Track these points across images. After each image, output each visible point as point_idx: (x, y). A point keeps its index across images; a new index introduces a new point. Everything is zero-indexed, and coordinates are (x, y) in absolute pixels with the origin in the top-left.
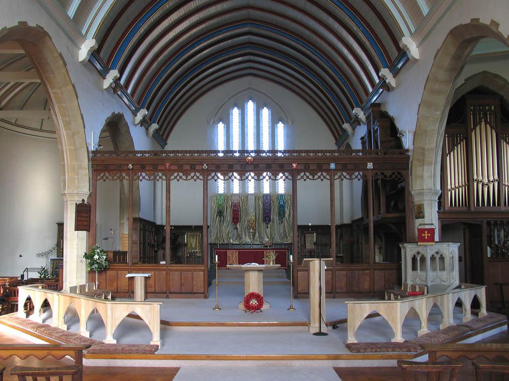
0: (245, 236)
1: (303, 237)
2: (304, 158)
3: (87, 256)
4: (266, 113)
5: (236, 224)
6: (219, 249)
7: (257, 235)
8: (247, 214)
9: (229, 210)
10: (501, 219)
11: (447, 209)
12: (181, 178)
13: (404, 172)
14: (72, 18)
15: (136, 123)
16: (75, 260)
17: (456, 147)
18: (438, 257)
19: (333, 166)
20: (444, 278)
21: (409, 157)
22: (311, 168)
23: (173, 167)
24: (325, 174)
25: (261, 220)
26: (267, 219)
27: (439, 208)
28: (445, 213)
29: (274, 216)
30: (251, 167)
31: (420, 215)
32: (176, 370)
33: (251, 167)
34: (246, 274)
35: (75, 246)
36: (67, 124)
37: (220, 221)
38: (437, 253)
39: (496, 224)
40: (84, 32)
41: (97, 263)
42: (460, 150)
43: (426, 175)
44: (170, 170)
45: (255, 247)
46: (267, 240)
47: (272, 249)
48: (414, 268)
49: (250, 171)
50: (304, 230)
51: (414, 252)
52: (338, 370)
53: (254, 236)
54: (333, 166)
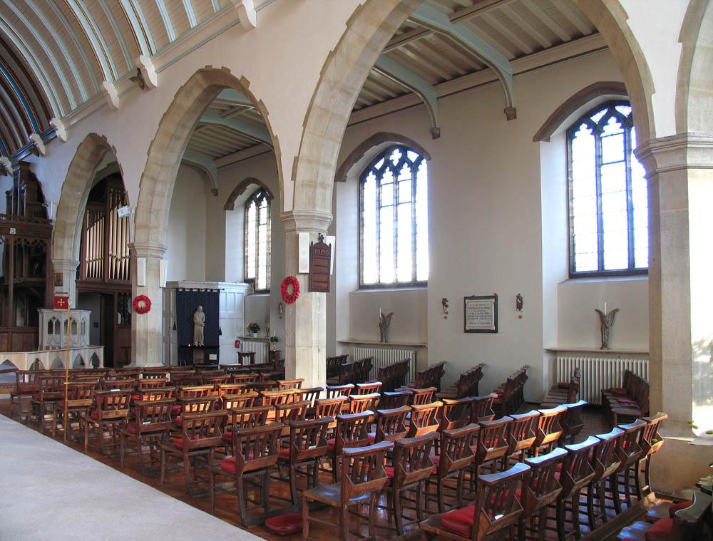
11: (84, 279)
27: (77, 278)
28: (82, 282)
31: (59, 282)
43: (66, 246)
48: (50, 332)
51: (50, 317)
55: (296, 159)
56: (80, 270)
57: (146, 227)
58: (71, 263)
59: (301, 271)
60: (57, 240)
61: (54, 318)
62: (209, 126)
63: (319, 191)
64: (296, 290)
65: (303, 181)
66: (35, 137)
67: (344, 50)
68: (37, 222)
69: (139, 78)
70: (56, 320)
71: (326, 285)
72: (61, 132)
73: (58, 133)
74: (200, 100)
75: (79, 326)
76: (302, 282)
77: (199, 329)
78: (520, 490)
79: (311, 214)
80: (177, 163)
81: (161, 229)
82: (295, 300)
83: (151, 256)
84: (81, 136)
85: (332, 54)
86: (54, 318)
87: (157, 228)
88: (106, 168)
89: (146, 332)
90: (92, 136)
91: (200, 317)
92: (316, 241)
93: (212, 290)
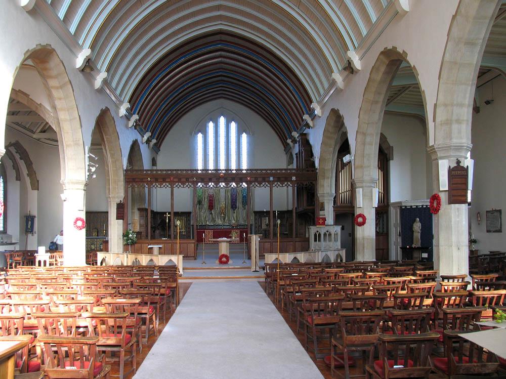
0: (218, 219)
1: (260, 219)
2: (255, 174)
3: (124, 236)
4: (233, 125)
5: (211, 210)
6: (199, 229)
7: (227, 218)
8: (219, 202)
9: (206, 200)
11: (338, 204)
12: (180, 186)
13: (314, 182)
14: (73, 34)
15: (144, 142)
16: (116, 237)
18: (328, 234)
19: (271, 179)
20: (331, 246)
21: (317, 173)
22: (259, 179)
23: (175, 180)
24: (267, 183)
25: (230, 207)
26: (234, 206)
29: (239, 204)
30: (223, 179)
31: (323, 209)
32: (191, 283)
33: (223, 180)
34: (220, 244)
35: (116, 229)
36: (112, 155)
37: (200, 208)
38: (327, 231)
40: (81, 42)
41: (131, 239)
43: (326, 185)
44: (173, 182)
45: (225, 227)
46: (234, 222)
47: (238, 229)
48: (315, 240)
49: (222, 182)
50: (260, 214)
51: (315, 231)
52: (259, 282)
53: (224, 219)
54: (271, 179)
55: (435, 105)
56: (336, 199)
57: (362, 167)
58: (329, 195)
59: (441, 189)
60: (320, 181)
61: (317, 232)
62: (414, 86)
63: (455, 127)
64: (439, 204)
65: (441, 121)
66: (306, 117)
67: (463, 11)
68: (308, 171)
69: (349, 68)
70: (328, 233)
71: (122, 212)
72: (318, 111)
73: (316, 112)
74: (386, 73)
75: (333, 236)
76: (444, 197)
77: (417, 235)
78: (483, 357)
79: (448, 145)
80: (379, 119)
81: (372, 167)
82: (438, 211)
83: (366, 186)
84: (327, 113)
85: (454, 17)
86: (317, 232)
89: (363, 238)
90: (333, 110)
91: (417, 226)
92: (454, 165)
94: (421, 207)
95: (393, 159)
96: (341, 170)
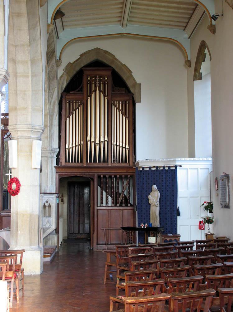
10: (104, 174)
11: (63, 164)
17: (74, 112)
27: (57, 163)
28: (62, 167)
39: (121, 177)
42: (77, 115)
77: (155, 210)
87: (25, 109)
88: (79, 59)
91: (154, 197)
93: (169, 167)
94: (162, 168)
95: (140, 102)
96: (69, 114)
